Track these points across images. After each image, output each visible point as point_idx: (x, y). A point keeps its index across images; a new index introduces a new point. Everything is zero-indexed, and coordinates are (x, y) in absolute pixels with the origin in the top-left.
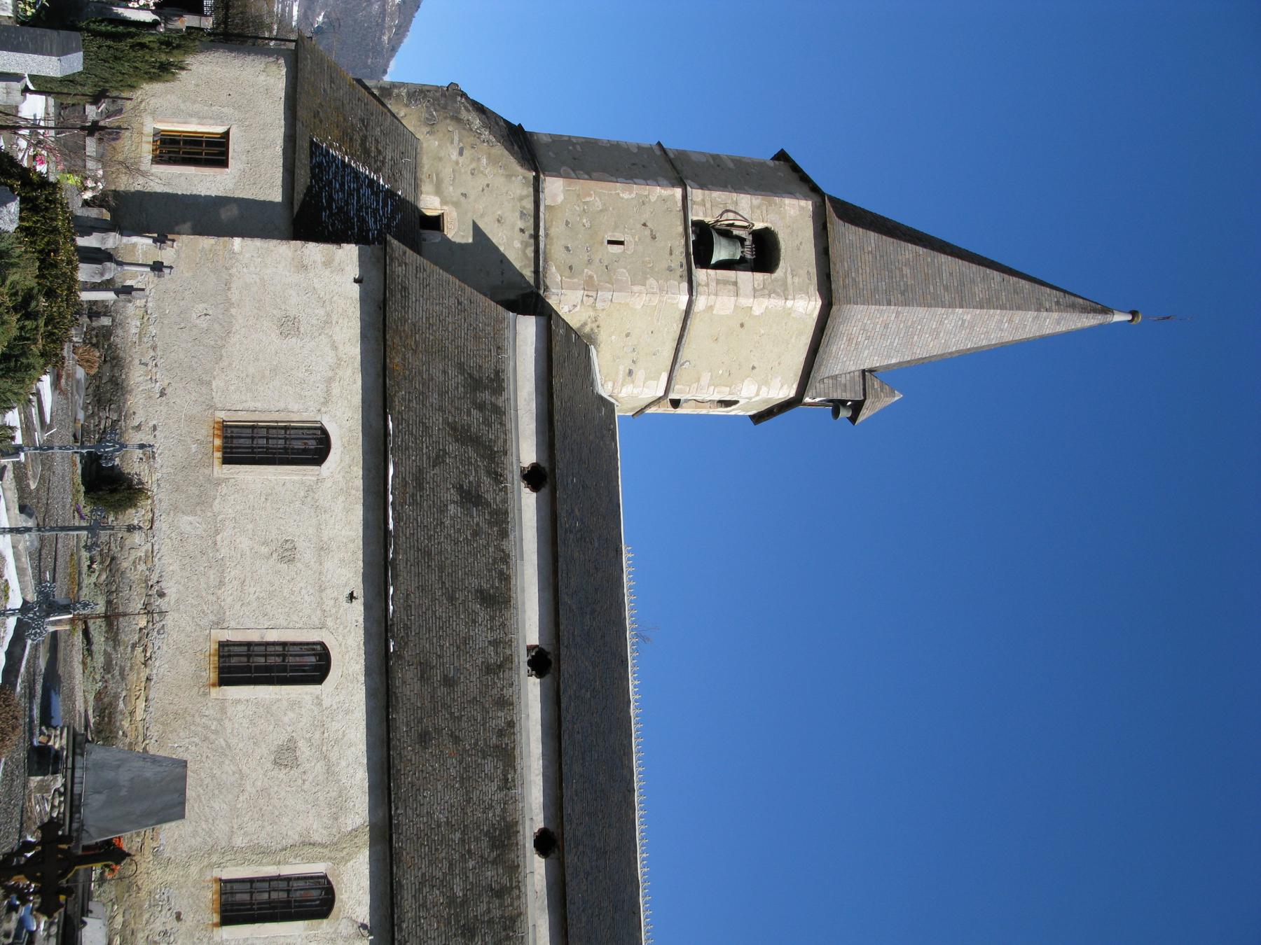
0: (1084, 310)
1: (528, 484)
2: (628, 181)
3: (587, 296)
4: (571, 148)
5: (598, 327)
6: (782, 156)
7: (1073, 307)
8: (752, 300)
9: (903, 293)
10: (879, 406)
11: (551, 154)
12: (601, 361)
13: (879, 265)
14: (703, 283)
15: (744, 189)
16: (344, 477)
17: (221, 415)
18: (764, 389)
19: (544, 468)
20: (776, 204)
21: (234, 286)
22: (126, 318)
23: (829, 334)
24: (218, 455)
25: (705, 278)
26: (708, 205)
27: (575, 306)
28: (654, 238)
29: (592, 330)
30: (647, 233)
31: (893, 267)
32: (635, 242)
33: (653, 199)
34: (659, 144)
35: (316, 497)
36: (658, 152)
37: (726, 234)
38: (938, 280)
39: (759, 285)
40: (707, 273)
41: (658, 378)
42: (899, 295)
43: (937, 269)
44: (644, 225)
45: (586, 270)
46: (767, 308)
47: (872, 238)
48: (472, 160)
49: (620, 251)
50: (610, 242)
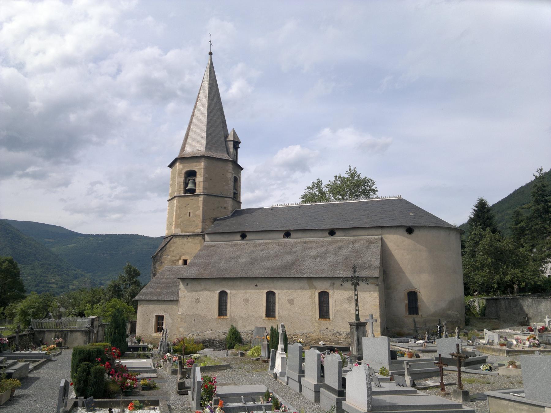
18: (229, 171)
26: (180, 190)
27: (206, 225)
30: (188, 206)
50: (190, 216)
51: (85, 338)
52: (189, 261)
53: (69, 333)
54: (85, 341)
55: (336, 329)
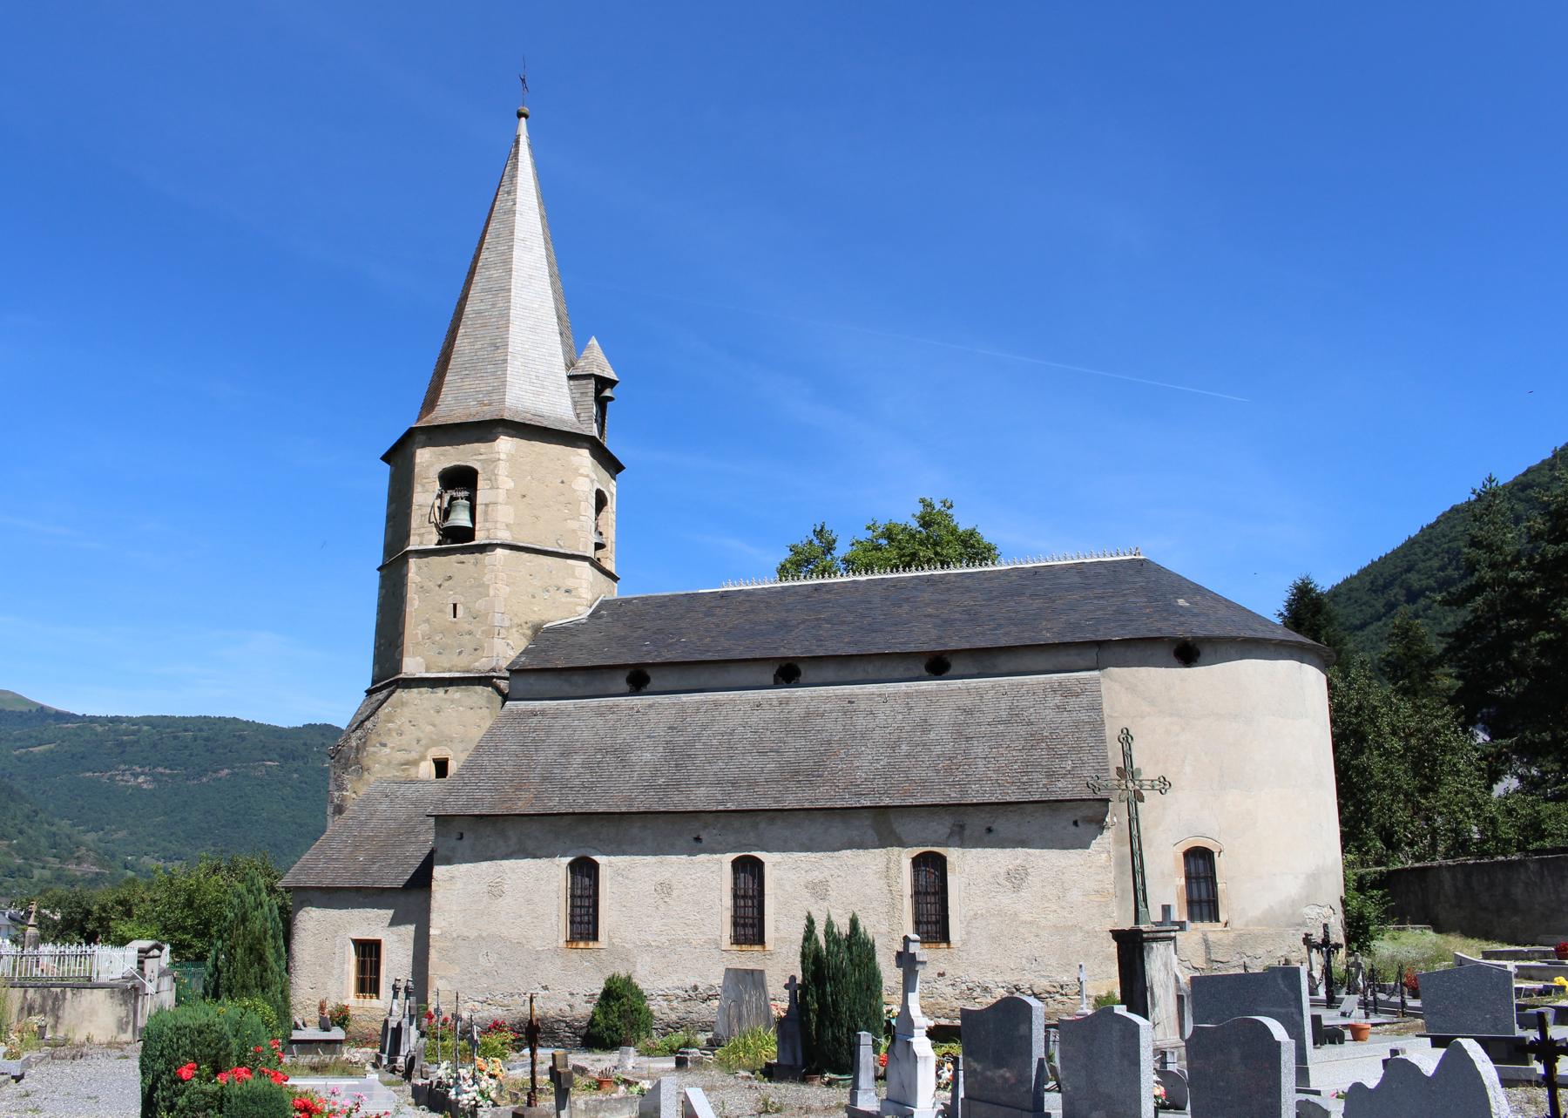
0: (515, 167)
6: (386, 458)
7: (513, 177)
8: (500, 491)
9: (497, 348)
10: (602, 359)
11: (387, 666)
12: (557, 617)
13: (473, 372)
14: (487, 534)
16: (608, 846)
17: (562, 943)
18: (581, 471)
19: (631, 673)
20: (421, 471)
21: (466, 934)
22: (490, 1017)
23: (531, 417)
24: (591, 944)
25: (483, 532)
27: (508, 644)
28: (450, 578)
30: (446, 584)
31: (475, 357)
33: (418, 579)
34: (378, 569)
35: (623, 867)
36: (385, 571)
37: (446, 514)
38: (487, 314)
41: (573, 567)
42: (499, 351)
43: (478, 315)
44: (440, 586)
45: (478, 636)
46: (507, 476)
47: (450, 378)
48: (390, 735)
50: (455, 616)
51: (121, 1011)
52: (452, 767)
53: (69, 993)
54: (120, 1020)
55: (974, 976)
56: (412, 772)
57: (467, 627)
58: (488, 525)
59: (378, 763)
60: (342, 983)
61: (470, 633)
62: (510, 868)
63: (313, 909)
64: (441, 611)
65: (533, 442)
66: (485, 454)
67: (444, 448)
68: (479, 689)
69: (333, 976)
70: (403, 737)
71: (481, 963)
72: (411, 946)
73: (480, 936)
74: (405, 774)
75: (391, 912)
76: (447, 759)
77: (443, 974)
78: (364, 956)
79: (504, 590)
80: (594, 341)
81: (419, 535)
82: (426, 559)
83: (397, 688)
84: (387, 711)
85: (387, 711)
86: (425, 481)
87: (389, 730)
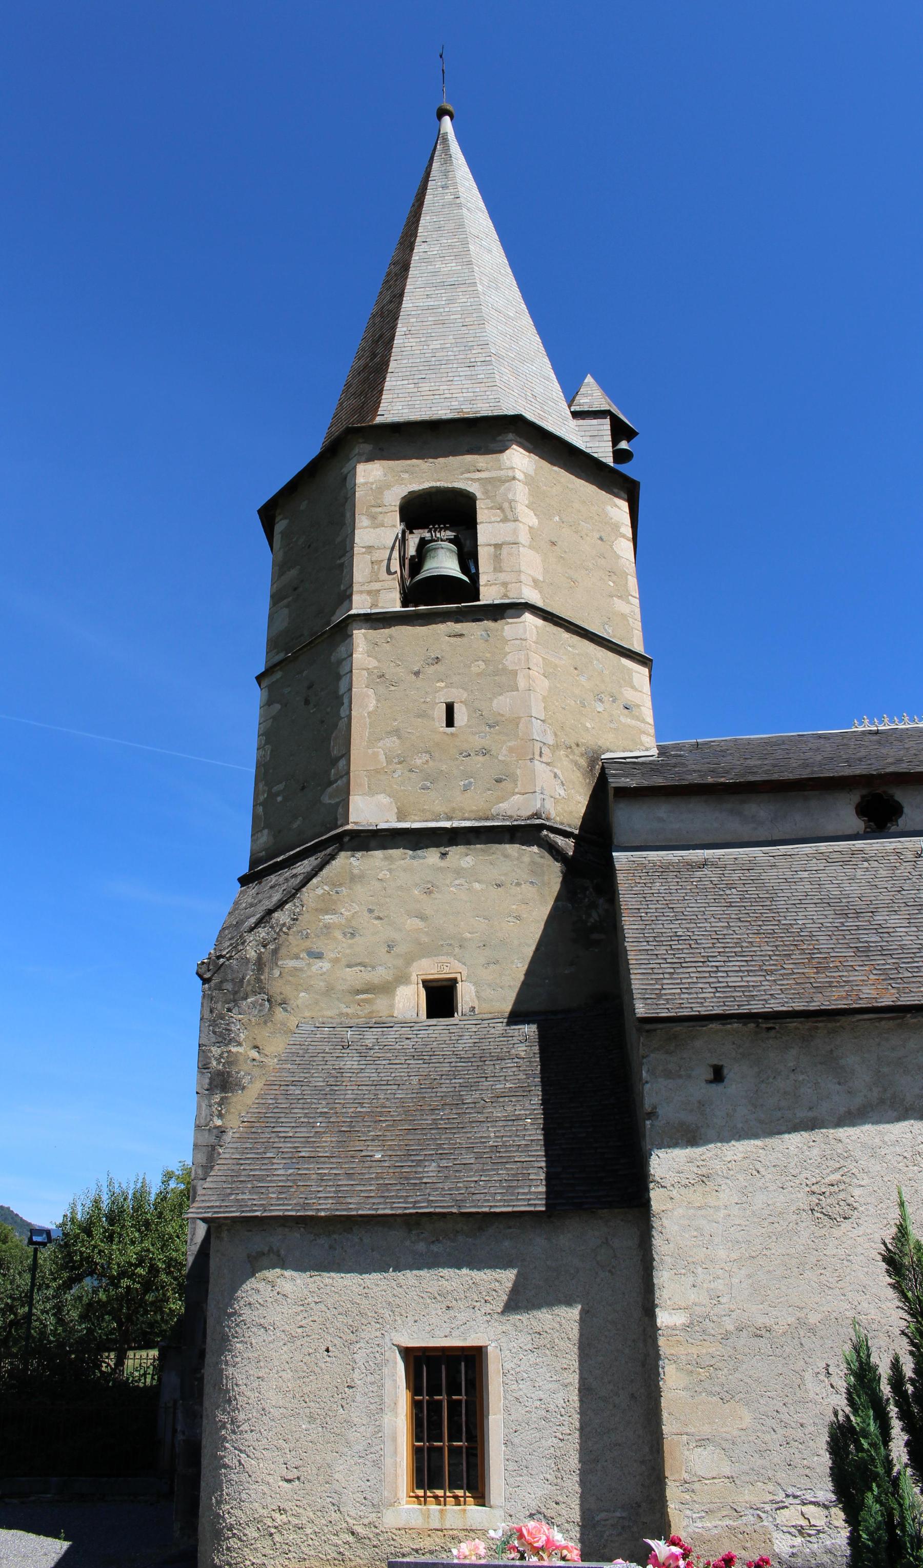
1: (891, 820)
2: (346, 701)
3: (541, 756)
4: (279, 799)
5: (578, 745)
14: (503, 590)
15: (344, 541)
19: (863, 797)
21: (761, 1321)
27: (556, 776)
29: (582, 755)
30: (431, 670)
32: (446, 687)
33: (373, 663)
34: (259, 678)
37: (416, 564)
39: (495, 515)
40: (486, 585)
41: (630, 671)
45: (500, 758)
49: (464, 709)
50: (450, 722)
56: (380, 1005)
57: (477, 742)
58: (503, 577)
59: (306, 990)
60: (377, 1464)
61: (485, 752)
62: (864, 1145)
63: (288, 1273)
64: (423, 715)
65: (556, 468)
66: (487, 469)
67: (409, 462)
68: (513, 849)
69: (348, 1444)
70: (357, 938)
71: (811, 1395)
72: (572, 1359)
73: (801, 1322)
74: (368, 1009)
75: (508, 1277)
76: (454, 981)
77: (706, 1430)
78: (434, 1389)
79: (542, 685)
80: (589, 379)
81: (369, 593)
82: (386, 631)
83: (341, 849)
84: (319, 891)
85: (319, 891)
86: (374, 510)
87: (327, 927)
